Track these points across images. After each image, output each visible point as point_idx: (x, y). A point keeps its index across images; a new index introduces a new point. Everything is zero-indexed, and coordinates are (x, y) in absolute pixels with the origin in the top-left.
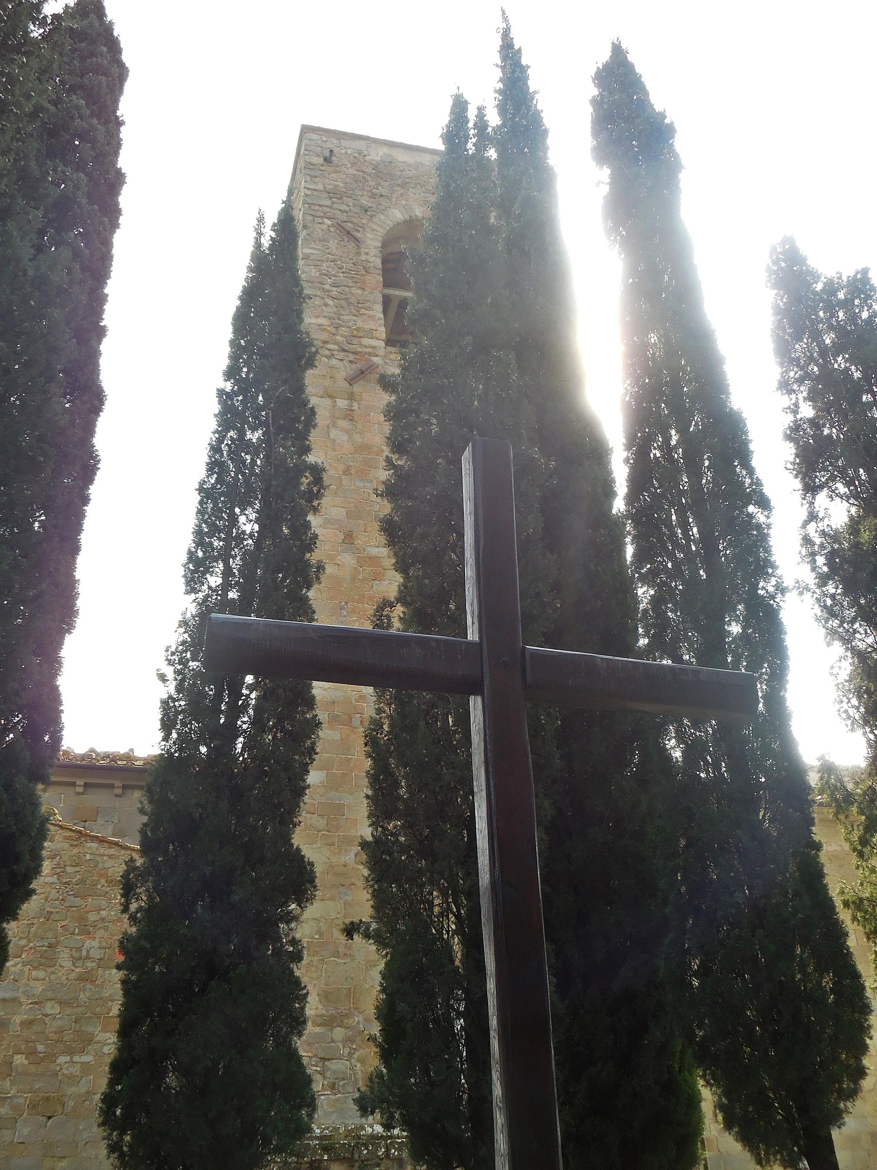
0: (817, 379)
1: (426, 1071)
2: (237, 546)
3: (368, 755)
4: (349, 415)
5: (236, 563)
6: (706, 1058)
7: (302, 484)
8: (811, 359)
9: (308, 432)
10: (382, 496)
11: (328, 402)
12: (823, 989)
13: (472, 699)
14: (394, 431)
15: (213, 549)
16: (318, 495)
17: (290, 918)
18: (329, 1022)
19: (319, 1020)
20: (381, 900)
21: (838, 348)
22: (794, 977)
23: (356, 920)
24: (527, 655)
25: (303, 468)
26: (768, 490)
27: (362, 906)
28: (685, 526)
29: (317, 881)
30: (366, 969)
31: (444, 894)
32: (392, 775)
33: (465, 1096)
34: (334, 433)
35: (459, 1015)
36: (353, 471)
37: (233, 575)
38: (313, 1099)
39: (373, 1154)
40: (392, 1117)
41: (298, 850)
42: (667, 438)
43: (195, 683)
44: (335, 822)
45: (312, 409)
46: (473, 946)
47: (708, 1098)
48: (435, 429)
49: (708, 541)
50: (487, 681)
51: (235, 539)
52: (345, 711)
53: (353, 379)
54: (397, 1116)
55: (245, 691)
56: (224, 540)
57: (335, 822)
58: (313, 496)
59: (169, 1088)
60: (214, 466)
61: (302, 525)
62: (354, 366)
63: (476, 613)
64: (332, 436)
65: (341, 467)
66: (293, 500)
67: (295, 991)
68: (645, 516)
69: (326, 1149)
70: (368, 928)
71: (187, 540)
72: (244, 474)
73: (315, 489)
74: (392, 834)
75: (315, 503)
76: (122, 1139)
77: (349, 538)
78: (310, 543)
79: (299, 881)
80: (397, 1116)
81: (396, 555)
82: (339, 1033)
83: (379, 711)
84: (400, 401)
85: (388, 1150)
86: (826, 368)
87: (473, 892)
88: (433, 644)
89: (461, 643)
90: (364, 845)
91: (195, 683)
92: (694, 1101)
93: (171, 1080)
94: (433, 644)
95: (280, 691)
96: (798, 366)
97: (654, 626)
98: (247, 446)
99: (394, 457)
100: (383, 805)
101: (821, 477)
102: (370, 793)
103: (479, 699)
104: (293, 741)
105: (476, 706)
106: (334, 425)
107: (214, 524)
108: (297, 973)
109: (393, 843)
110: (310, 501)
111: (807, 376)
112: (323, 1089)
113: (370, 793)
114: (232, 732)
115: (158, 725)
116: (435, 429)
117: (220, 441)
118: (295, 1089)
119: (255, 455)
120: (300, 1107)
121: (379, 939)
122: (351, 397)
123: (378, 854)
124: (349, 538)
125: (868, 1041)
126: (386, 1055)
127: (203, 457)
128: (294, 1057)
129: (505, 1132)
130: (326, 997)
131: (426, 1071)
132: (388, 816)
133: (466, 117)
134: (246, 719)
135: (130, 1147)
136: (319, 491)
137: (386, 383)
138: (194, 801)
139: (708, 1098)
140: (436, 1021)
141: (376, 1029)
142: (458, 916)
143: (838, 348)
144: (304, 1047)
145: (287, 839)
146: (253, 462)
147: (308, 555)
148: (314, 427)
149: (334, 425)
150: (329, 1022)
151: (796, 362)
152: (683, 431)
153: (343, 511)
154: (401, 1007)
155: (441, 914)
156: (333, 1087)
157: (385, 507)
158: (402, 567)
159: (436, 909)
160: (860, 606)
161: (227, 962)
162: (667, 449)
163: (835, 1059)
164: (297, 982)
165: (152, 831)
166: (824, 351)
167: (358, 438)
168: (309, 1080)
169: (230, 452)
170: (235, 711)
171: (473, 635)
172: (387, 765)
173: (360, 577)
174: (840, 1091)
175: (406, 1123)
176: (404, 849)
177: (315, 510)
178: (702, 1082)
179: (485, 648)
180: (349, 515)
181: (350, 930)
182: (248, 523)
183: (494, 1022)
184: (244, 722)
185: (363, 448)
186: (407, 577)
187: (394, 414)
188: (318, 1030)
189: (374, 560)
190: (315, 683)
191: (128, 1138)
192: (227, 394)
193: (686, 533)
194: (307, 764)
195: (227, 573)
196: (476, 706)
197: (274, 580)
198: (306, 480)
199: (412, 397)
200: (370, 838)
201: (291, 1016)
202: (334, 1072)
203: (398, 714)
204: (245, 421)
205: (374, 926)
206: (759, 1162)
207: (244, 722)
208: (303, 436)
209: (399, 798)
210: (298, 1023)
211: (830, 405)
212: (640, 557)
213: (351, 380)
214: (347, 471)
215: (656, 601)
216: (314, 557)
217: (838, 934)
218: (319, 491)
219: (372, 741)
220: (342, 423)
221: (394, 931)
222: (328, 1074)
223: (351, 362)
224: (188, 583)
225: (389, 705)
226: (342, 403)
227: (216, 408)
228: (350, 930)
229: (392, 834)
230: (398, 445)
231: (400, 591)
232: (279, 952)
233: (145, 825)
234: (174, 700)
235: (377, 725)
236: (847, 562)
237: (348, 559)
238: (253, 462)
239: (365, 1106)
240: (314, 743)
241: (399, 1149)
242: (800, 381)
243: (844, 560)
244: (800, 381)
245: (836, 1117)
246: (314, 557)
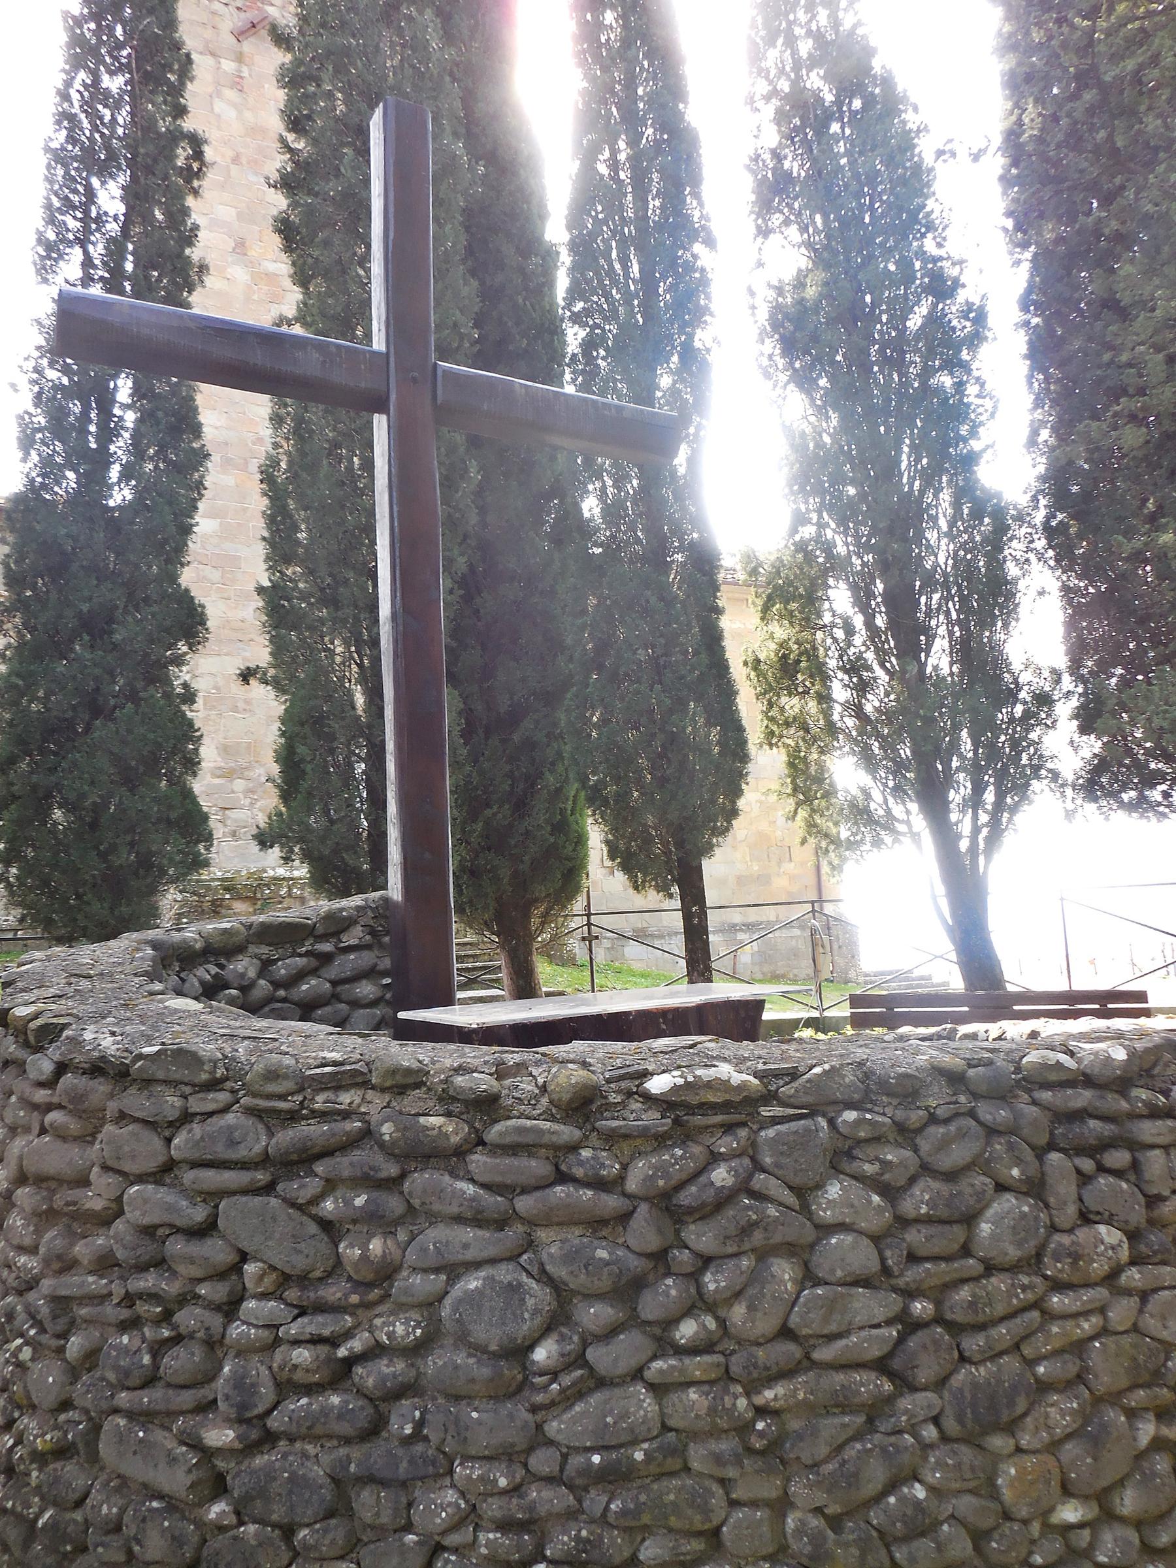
0: (786, 98)
1: (326, 812)
2: (98, 230)
3: (265, 494)
4: (237, 83)
5: (97, 251)
6: (596, 799)
7: (177, 157)
8: (782, 71)
9: (182, 84)
10: (275, 187)
11: (210, 61)
12: (710, 742)
13: (376, 416)
14: (290, 100)
15: (68, 230)
16: (199, 175)
17: (179, 661)
18: (229, 775)
19: (219, 772)
20: (279, 647)
21: (813, 62)
22: (684, 729)
23: (252, 665)
24: (439, 373)
25: (176, 136)
26: (716, 227)
27: (260, 654)
28: (624, 261)
29: (209, 624)
30: (266, 708)
31: (346, 643)
32: (291, 517)
33: (365, 834)
34: (219, 106)
35: (361, 759)
36: (244, 160)
37: (95, 267)
38: (211, 834)
39: (276, 893)
40: (291, 851)
41: (187, 591)
42: (614, 152)
43: (54, 397)
44: (227, 559)
45: (188, 55)
46: (375, 695)
47: (596, 837)
48: (341, 108)
49: (648, 282)
50: (393, 397)
51: (92, 222)
52: (237, 425)
53: (242, 33)
54: (296, 850)
55: (117, 411)
56: (81, 220)
57: (227, 559)
58: (193, 174)
59: (56, 824)
60: (66, 118)
61: (180, 211)
62: (242, 15)
63: (383, 318)
64: (217, 110)
65: (230, 154)
66: (166, 177)
67: (187, 733)
68: (585, 249)
69: (227, 889)
70: (265, 674)
71: (36, 218)
72: (102, 135)
73: (195, 166)
74: (291, 580)
75: (196, 183)
76: (8, 872)
77: (240, 246)
78: (189, 238)
79: (189, 622)
80: (296, 850)
81: (294, 264)
82: (239, 785)
83: (276, 446)
84: (298, 63)
85: (290, 889)
86: (797, 82)
87: (375, 642)
88: (333, 350)
89: (364, 351)
90: (261, 590)
91: (54, 397)
92: (580, 840)
93: (58, 814)
94: (333, 350)
95: (160, 414)
96: (767, 78)
97: (583, 372)
98: (105, 97)
99: (290, 137)
100: (280, 546)
101: (776, 219)
102: (266, 534)
103: (384, 417)
104: (179, 472)
105: (380, 424)
106: (219, 95)
107: (67, 198)
108: (189, 714)
109: (293, 589)
110: (188, 181)
111: (775, 92)
112: (224, 835)
113: (266, 534)
114: (102, 459)
115: (15, 444)
116: (341, 108)
117: (68, 84)
118: (192, 825)
119: (116, 106)
120: (198, 842)
121: (277, 684)
122: (240, 58)
123: (278, 606)
124: (240, 246)
125: (744, 786)
126: (285, 796)
127: (49, 105)
128: (188, 795)
129: (399, 843)
130: (225, 750)
131: (326, 812)
132: (287, 560)
133: (1064, 557)
134: (121, 444)
135: (18, 878)
136: (200, 170)
137: (280, 39)
138: (64, 531)
139: (596, 837)
140: (336, 765)
141: (275, 769)
142: (360, 666)
143: (813, 62)
144: (201, 786)
145: (173, 578)
146: (114, 120)
147: (188, 251)
148: (192, 79)
149: (219, 95)
150: (229, 775)
151: (763, 73)
152: (633, 143)
153: (233, 212)
154: (301, 750)
155: (343, 663)
156: (234, 834)
157: (279, 202)
158: (302, 278)
159: (338, 659)
160: (795, 370)
161: (112, 702)
162: (614, 165)
163: (713, 801)
164: (190, 724)
165: (16, 562)
166: (797, 65)
167: (248, 115)
168: (205, 818)
169: (84, 102)
170: (108, 433)
171: (379, 343)
172: (285, 506)
173: (255, 297)
174: (714, 829)
175: (307, 856)
176: (304, 597)
177: (196, 192)
178: (590, 820)
179: (392, 359)
180: (240, 216)
181: (246, 676)
182: (110, 198)
183: (390, 746)
184: (119, 447)
185: (255, 131)
186: (307, 293)
187: (292, 79)
188: (217, 781)
189: (270, 277)
190: (202, 386)
191: (14, 871)
192: (74, 18)
193: (626, 268)
194: (195, 500)
195: (87, 263)
196: (380, 424)
197: (147, 278)
198: (182, 155)
199: (313, 59)
200: (267, 584)
201: (184, 757)
202: (236, 821)
203: (297, 450)
204: (100, 61)
205: (272, 672)
206: (636, 888)
207: (119, 447)
208: (177, 91)
209: (298, 543)
210: (192, 763)
211: (796, 129)
212: (575, 292)
213: (239, 35)
214: (236, 160)
215: (589, 345)
216: (195, 254)
217: (728, 692)
218: (200, 170)
219: (268, 476)
220: (230, 94)
221: (292, 678)
222: (229, 822)
223: (239, 9)
224: (38, 272)
225: (287, 439)
226: (228, 66)
227: (63, 38)
228: (246, 676)
229: (291, 580)
230: (296, 123)
231: (299, 309)
232: (169, 696)
233: (7, 556)
234: (30, 415)
235: (274, 463)
236: (790, 320)
237: (239, 274)
238: (114, 120)
239: (264, 840)
240: (202, 477)
241: (302, 889)
242: (767, 98)
243: (787, 316)
244: (767, 98)
245: (708, 849)
246: (195, 254)
